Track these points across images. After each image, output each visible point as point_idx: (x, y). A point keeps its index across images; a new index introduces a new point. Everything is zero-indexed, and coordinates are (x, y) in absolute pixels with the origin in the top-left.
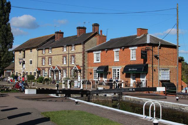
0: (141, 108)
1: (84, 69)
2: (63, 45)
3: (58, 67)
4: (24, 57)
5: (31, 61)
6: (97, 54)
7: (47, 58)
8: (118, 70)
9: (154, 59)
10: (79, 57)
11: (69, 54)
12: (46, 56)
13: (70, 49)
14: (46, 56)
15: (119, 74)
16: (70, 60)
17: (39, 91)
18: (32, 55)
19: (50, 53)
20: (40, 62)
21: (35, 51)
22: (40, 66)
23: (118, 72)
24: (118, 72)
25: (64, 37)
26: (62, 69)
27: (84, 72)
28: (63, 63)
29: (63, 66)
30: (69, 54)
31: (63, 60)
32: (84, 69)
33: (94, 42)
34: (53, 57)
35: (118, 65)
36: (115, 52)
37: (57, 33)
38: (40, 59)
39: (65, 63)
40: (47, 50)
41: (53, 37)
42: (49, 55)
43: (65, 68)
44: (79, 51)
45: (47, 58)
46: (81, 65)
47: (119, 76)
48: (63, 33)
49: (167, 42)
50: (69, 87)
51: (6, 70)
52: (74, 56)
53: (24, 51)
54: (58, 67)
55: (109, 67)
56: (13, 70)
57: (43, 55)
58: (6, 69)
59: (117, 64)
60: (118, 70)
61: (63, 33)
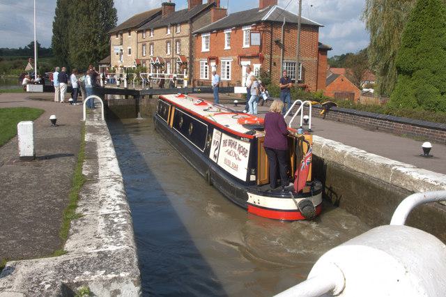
0: (121, 158)
1: (191, 61)
2: (165, 24)
3: (160, 59)
5: (130, 53)
6: (207, 37)
7: (148, 44)
8: (228, 63)
9: (274, 46)
10: (185, 42)
11: (173, 38)
13: (175, 29)
15: (230, 69)
17: (232, 91)
18: (131, 38)
19: (152, 36)
20: (140, 52)
21: (134, 33)
22: (140, 57)
23: (228, 67)
24: (228, 67)
25: (176, 11)
26: (165, 62)
27: (191, 66)
28: (167, 52)
29: (166, 57)
30: (173, 38)
31: (167, 47)
32: (191, 61)
33: (210, 19)
34: (155, 43)
35: (229, 56)
36: (226, 35)
37: (164, 4)
38: (140, 45)
39: (169, 53)
40: (148, 33)
41: (159, 13)
42: (151, 39)
43: (168, 60)
45: (148, 44)
46: (188, 55)
47: (230, 72)
48: (174, 5)
49: (355, 244)
50: (125, 86)
51: (101, 64)
52: (178, 41)
53: (122, 35)
54: (160, 59)
56: (109, 64)
57: (143, 40)
58: (101, 62)
60: (228, 63)
61: (174, 5)
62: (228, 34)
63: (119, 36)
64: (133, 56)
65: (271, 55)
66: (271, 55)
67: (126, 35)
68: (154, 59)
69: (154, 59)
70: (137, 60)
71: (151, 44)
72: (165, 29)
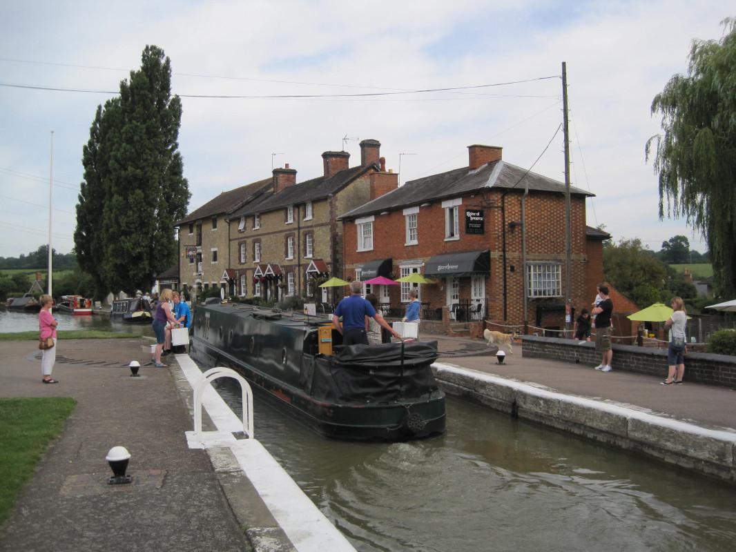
4: (200, 244)
7: (249, 241)
11: (299, 228)
12: (247, 237)
14: (247, 237)
16: (302, 247)
20: (234, 256)
22: (235, 265)
34: (263, 239)
38: (235, 244)
39: (291, 257)
43: (289, 269)
44: (323, 221)
45: (249, 241)
46: (328, 259)
55: (395, 262)
59: (411, 253)
61: (294, 172)
62: (413, 216)
63: (195, 230)
64: (222, 262)
65: (504, 251)
66: (504, 251)
67: (207, 229)
68: (264, 268)
69: (264, 268)
70: (230, 271)
71: (254, 242)
72: (282, 214)
